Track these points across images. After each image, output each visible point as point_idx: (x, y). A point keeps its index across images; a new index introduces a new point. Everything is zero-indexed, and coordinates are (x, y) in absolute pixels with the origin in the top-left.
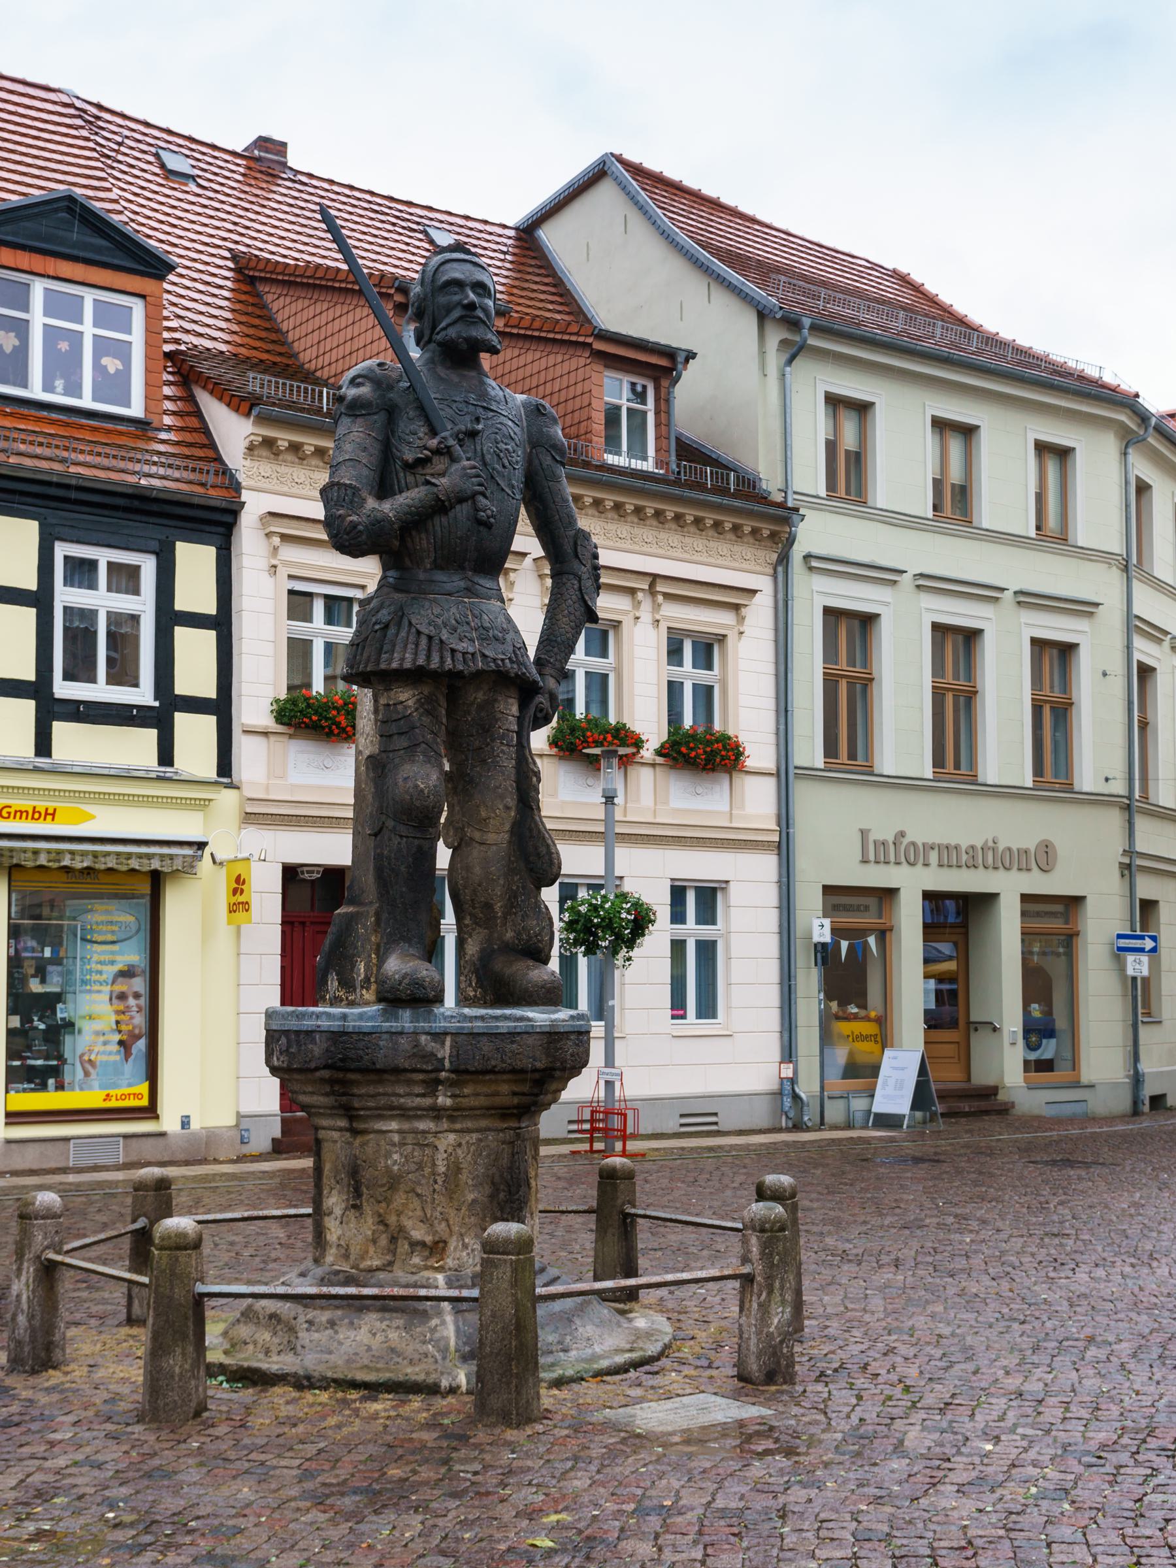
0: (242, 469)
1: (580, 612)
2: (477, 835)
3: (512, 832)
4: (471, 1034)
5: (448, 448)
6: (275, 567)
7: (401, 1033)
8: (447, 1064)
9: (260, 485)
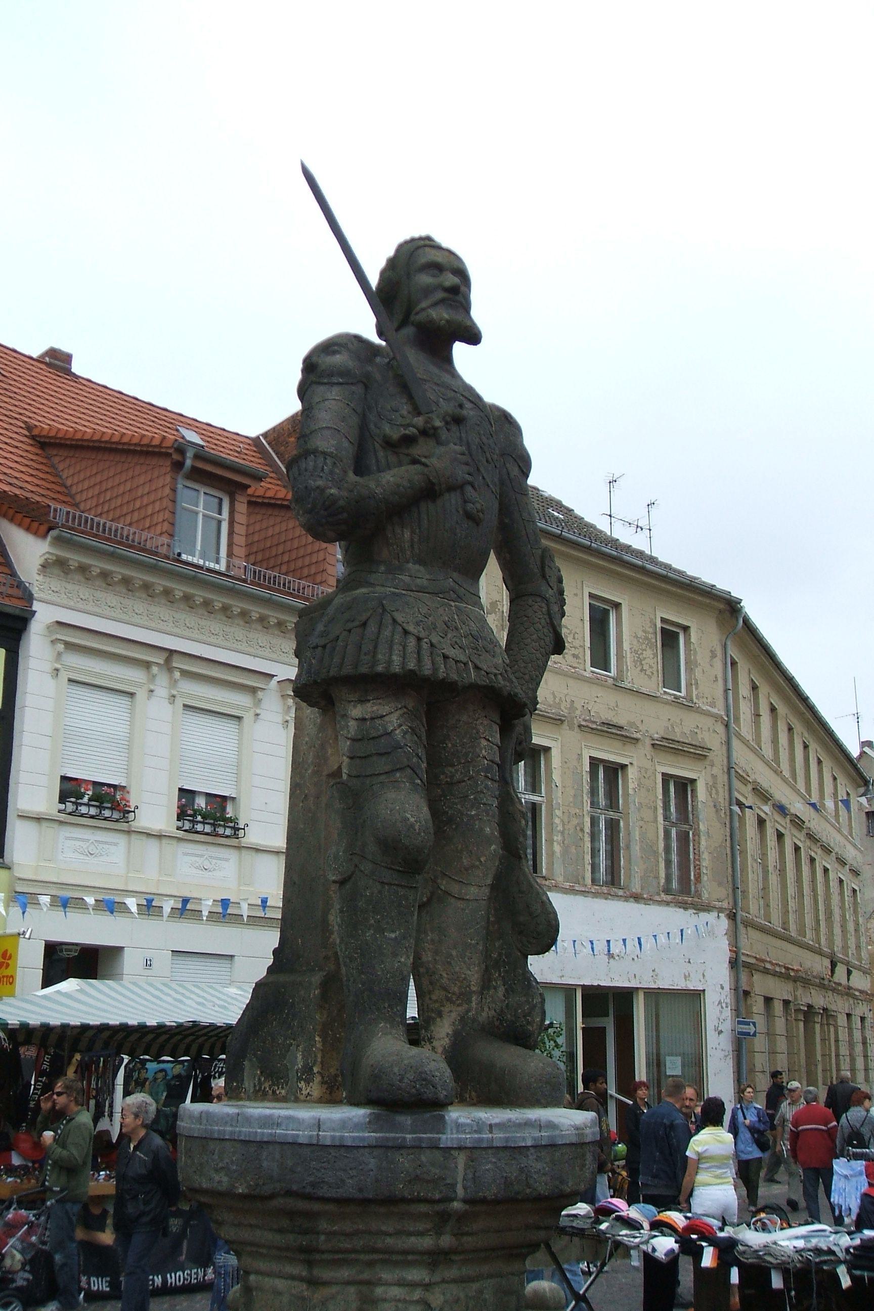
0: (36, 583)
1: (549, 639)
2: (455, 889)
3: (493, 887)
4: (505, 1148)
5: (435, 429)
6: (57, 670)
7: (400, 1148)
8: (460, 1192)
9: (49, 597)
